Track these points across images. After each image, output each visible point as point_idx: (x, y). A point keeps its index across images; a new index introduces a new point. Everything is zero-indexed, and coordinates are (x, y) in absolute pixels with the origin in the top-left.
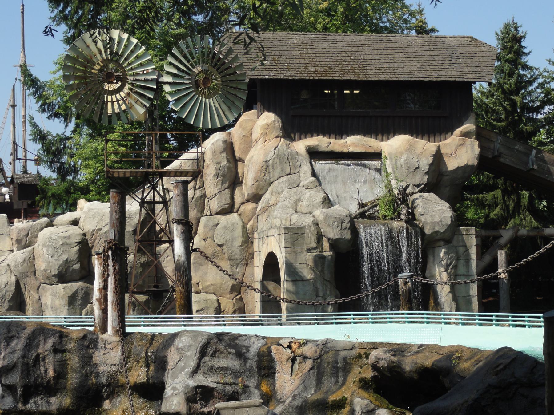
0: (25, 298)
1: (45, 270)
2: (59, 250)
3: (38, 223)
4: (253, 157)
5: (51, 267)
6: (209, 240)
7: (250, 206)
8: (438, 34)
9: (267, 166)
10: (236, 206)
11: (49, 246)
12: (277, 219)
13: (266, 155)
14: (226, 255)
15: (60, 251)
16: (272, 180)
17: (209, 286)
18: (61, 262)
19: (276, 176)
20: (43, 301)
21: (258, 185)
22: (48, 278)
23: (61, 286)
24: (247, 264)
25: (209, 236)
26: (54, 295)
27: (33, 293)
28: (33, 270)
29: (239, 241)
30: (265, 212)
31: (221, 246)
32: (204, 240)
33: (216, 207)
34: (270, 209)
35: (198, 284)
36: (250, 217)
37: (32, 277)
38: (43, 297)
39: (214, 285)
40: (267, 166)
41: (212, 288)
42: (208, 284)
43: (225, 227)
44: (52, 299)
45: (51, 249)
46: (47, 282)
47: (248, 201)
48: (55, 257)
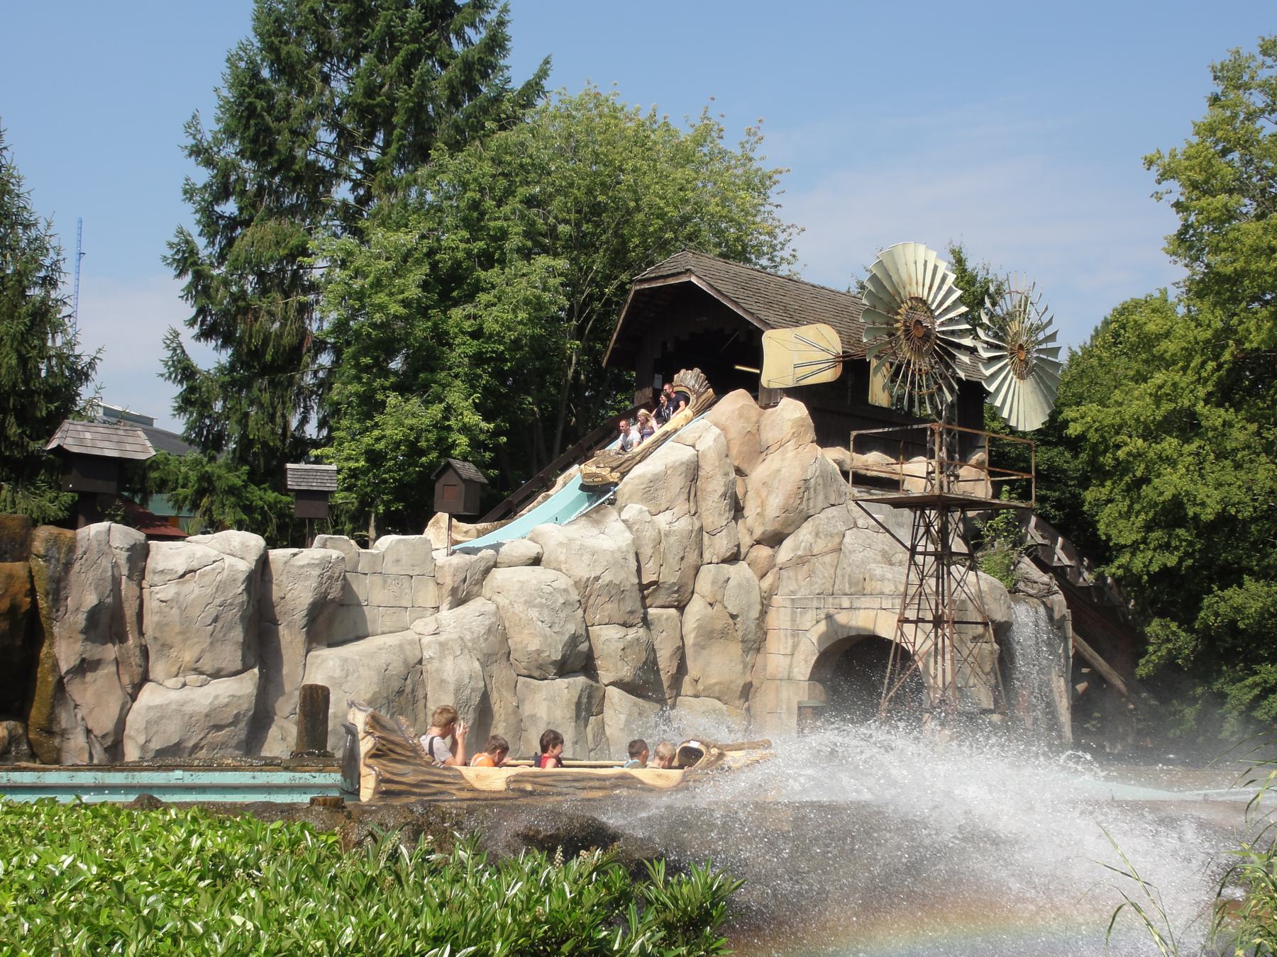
0: (492, 702)
1: (539, 652)
2: (560, 614)
3: (482, 558)
4: (779, 470)
5: (550, 645)
6: (717, 607)
7: (764, 552)
8: (194, 230)
9: (807, 489)
10: (743, 550)
11: (541, 606)
12: (886, 582)
13: (805, 470)
14: (740, 633)
15: (562, 615)
16: (811, 512)
17: (715, 684)
18: (566, 637)
19: (820, 505)
20: (527, 710)
21: (787, 518)
22: (540, 667)
23: (562, 683)
24: (758, 650)
25: (719, 598)
26: (552, 699)
27: (508, 695)
28: (505, 650)
29: (755, 613)
30: (804, 564)
31: (733, 617)
32: (711, 604)
33: (724, 550)
34: (814, 560)
35: (697, 681)
36: (764, 570)
37: (504, 662)
38: (527, 702)
39: (720, 683)
40: (807, 489)
41: (717, 688)
42: (713, 681)
43: (740, 586)
44: (549, 708)
45: (546, 611)
46: (536, 674)
47: (758, 542)
48: (556, 629)
